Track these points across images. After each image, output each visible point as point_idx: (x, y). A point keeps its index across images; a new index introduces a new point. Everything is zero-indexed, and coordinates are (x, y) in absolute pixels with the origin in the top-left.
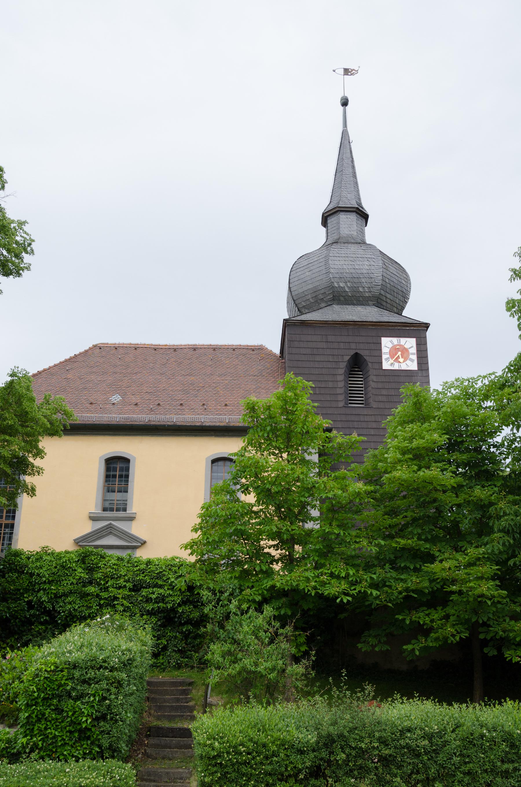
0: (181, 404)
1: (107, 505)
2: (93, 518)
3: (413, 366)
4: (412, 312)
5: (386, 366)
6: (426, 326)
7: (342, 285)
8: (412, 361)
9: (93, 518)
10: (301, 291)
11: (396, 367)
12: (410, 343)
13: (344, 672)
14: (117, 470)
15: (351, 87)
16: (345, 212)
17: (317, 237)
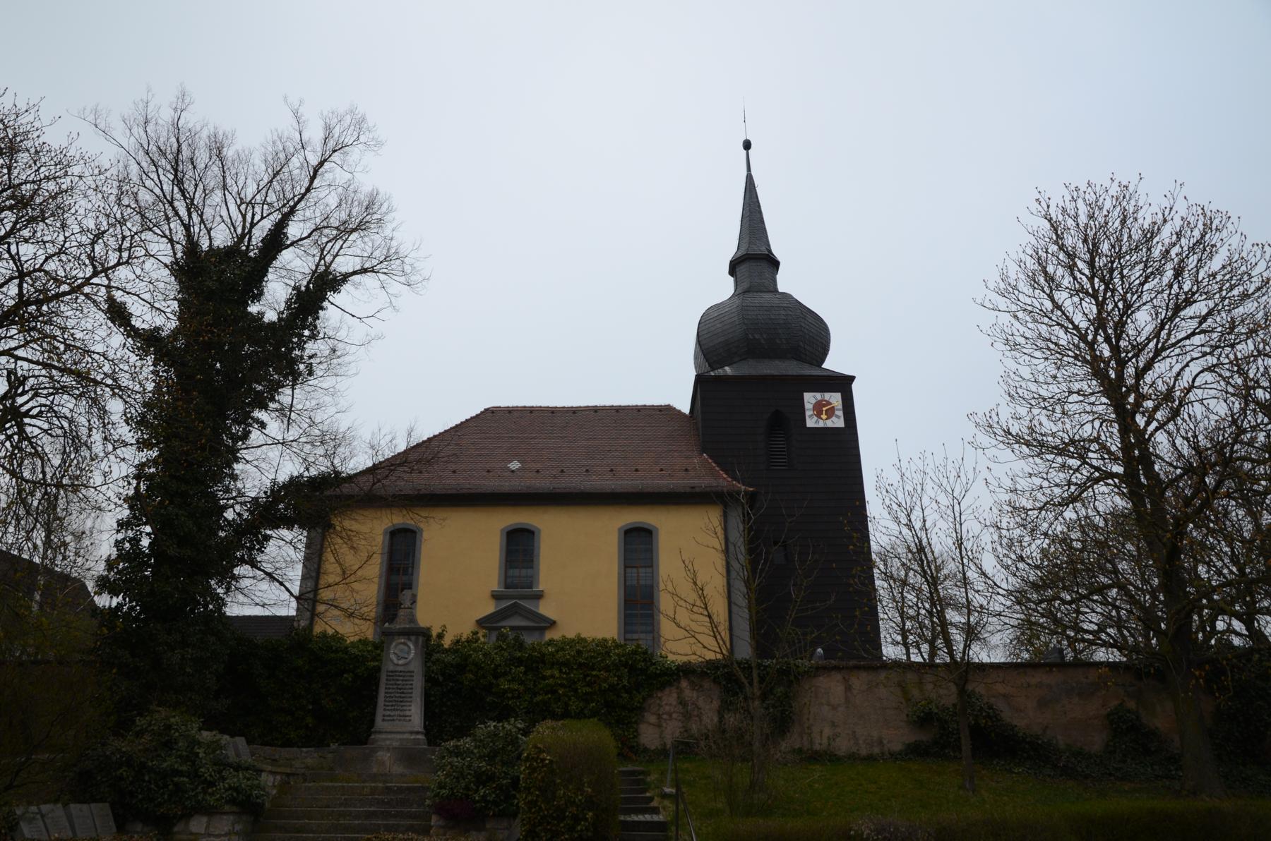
1: (509, 580)
2: (496, 596)
3: (70, 834)
4: (834, 363)
5: (811, 422)
6: (852, 378)
7: (757, 336)
8: (838, 417)
9: (496, 596)
11: (821, 424)
12: (835, 399)
14: (520, 546)
16: (754, 261)
17: (723, 288)
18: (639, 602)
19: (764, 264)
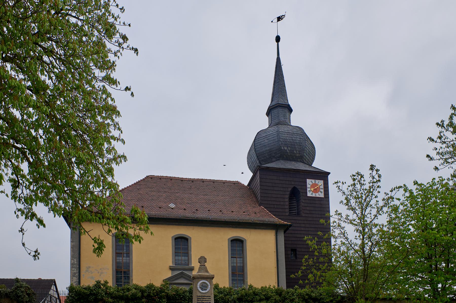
0: (209, 210)
2: (172, 269)
3: (322, 195)
4: (319, 164)
5: (309, 194)
8: (321, 192)
9: (172, 269)
10: (261, 151)
12: (320, 183)
14: (181, 244)
15: (282, 29)
16: (279, 108)
17: (264, 123)
18: (238, 273)
19: (286, 110)
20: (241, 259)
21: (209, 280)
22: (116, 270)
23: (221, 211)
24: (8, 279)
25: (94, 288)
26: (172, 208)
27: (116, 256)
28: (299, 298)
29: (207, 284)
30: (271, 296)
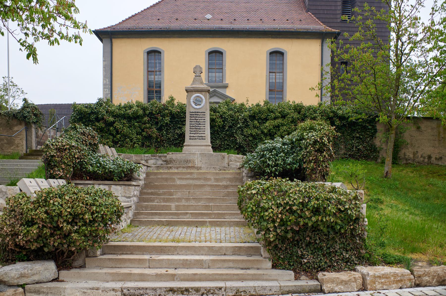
0: (248, 20)
13: (366, 171)
20: (281, 74)
21: (204, 93)
22: (148, 89)
23: (261, 20)
24: (65, 104)
25: (95, 106)
26: (208, 19)
27: (148, 75)
28: (322, 116)
29: (201, 98)
30: (288, 114)
